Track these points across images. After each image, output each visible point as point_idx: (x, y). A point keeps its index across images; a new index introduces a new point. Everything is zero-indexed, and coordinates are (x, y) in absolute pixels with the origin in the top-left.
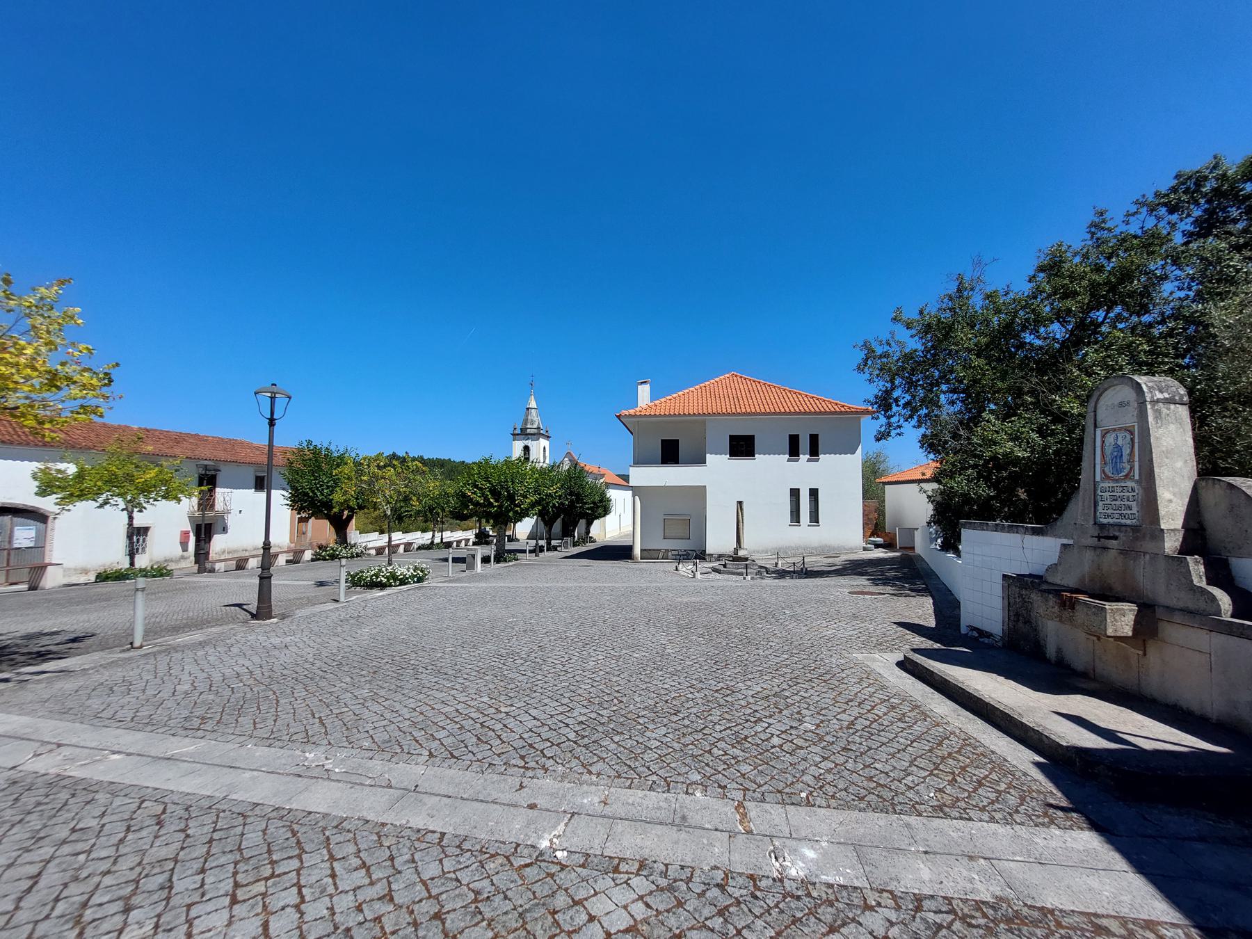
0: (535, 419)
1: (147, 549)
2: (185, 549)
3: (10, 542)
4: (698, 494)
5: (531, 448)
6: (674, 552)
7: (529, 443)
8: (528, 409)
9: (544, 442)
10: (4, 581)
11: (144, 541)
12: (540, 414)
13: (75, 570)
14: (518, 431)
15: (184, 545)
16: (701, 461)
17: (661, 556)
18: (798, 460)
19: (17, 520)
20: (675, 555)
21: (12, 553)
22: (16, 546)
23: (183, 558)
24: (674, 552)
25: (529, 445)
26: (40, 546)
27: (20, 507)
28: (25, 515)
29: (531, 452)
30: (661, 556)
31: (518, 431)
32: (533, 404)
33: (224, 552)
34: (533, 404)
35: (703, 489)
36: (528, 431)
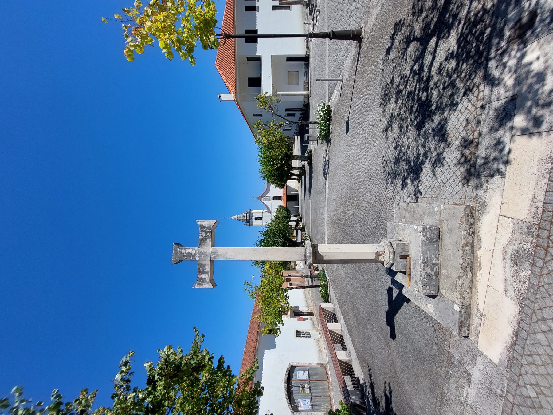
0: (242, 216)
1: (307, 331)
2: (308, 319)
3: (306, 380)
4: (275, 58)
5: (256, 217)
6: (305, 79)
7: (253, 218)
8: (238, 219)
9: (253, 212)
10: (326, 382)
11: (303, 333)
12: (240, 214)
13: (319, 354)
14: (248, 224)
15: (304, 319)
16: (258, 59)
17: (307, 86)
18: (258, 7)
19: (294, 378)
20: (306, 78)
21: (311, 379)
22: (308, 378)
23: (311, 320)
24: (305, 79)
25: (254, 218)
26: (308, 369)
27: (287, 376)
28: (291, 375)
29: (258, 217)
30: (307, 86)
31: (248, 224)
32: (235, 217)
33: (308, 307)
34: (235, 217)
35: (273, 57)
36: (248, 218)
